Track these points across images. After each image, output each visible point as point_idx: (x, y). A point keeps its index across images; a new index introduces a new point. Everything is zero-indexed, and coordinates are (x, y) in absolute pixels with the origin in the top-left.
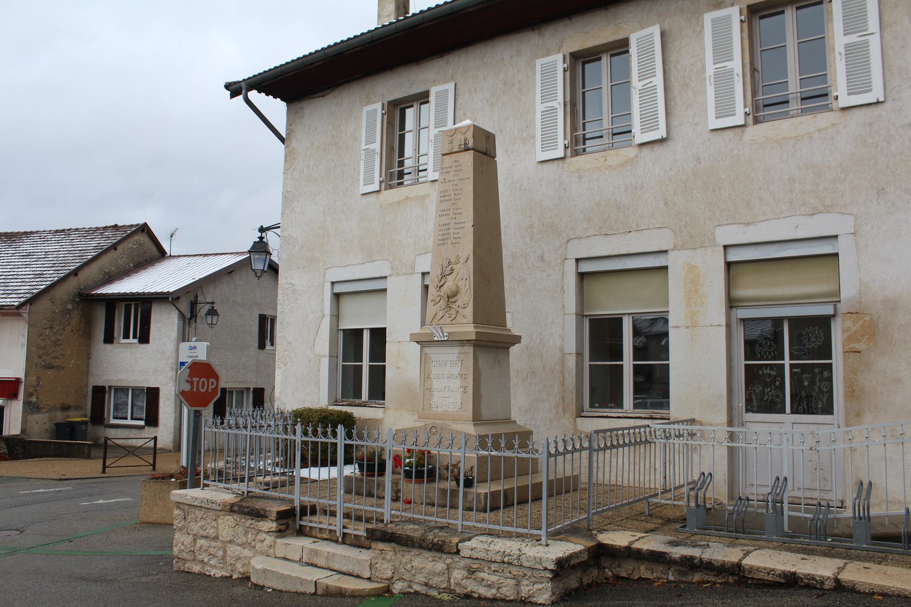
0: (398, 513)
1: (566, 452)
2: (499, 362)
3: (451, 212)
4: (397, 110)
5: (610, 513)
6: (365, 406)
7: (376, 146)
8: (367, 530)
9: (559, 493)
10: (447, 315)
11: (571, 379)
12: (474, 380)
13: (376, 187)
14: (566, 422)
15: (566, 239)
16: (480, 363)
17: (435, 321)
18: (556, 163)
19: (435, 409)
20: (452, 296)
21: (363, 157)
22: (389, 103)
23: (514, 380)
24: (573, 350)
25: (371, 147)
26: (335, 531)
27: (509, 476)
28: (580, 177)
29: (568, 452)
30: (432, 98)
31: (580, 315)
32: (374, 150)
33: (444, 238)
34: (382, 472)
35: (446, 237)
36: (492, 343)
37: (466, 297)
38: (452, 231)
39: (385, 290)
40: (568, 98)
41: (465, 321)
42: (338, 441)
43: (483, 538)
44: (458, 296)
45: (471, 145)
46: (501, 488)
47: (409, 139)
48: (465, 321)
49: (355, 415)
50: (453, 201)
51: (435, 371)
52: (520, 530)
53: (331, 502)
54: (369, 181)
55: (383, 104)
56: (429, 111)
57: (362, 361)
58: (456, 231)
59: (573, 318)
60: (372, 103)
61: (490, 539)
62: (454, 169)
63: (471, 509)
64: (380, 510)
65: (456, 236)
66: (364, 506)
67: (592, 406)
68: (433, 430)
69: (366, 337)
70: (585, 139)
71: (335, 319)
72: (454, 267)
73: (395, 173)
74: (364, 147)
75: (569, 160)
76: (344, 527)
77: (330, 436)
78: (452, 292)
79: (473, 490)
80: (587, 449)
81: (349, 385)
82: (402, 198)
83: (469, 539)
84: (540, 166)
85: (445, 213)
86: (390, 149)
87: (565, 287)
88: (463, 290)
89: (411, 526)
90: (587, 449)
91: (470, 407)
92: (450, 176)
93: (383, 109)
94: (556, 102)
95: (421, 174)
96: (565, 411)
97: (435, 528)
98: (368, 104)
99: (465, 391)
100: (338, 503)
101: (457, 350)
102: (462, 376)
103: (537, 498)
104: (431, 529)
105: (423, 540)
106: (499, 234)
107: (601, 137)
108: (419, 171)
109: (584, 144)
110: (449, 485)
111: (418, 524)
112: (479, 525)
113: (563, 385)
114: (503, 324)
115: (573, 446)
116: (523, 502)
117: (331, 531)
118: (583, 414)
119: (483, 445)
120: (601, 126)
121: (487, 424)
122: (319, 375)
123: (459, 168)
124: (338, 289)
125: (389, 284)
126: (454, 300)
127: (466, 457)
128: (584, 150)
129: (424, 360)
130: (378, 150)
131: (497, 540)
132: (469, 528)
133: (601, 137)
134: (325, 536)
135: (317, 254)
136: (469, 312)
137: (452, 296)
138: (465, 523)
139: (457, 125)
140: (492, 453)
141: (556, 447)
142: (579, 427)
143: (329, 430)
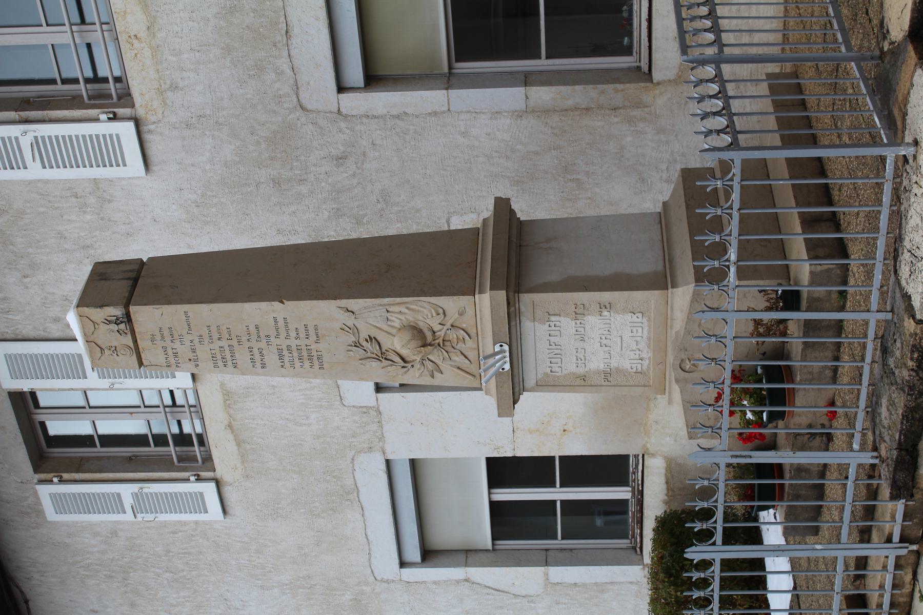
0: (858, 436)
1: (726, 111)
2: (548, 240)
3: (256, 346)
4: (53, 454)
5: (845, 11)
6: (641, 493)
7: (126, 491)
8: (894, 497)
9: (808, 122)
10: (461, 346)
11: (577, 95)
12: (586, 289)
13: (209, 489)
14: (660, 100)
15: (299, 112)
16: (554, 277)
17: (473, 369)
18: (147, 137)
19: (646, 363)
20: (422, 338)
21: (149, 517)
22: (37, 470)
23: (583, 208)
24: (520, 91)
25: (128, 501)
26: (898, 558)
27: (775, 223)
28: (174, 88)
29: (731, 124)
30: (25, 385)
31: (450, 80)
32: (135, 496)
33: (306, 357)
34: (776, 470)
35: (305, 353)
36: (512, 257)
37: (424, 310)
38: (293, 343)
39: (413, 462)
40: (12, 115)
41: (470, 312)
42: (718, 557)
43: (904, 270)
44: (422, 325)
45: (118, 312)
46: (801, 238)
47: (109, 427)
48: (470, 312)
49: (660, 512)
50: (234, 342)
51: (570, 366)
52: (886, 198)
53: (840, 567)
54: (198, 503)
55: (41, 482)
56: (51, 391)
57: (554, 502)
58: (293, 334)
59: (456, 94)
60: (38, 502)
61: (906, 256)
62: (168, 343)
63: (843, 294)
64: (852, 472)
65: (302, 335)
66: (843, 502)
67: (628, 51)
68: (688, 366)
69: (506, 495)
70: (96, 79)
71: (472, 558)
72: (364, 335)
73: (177, 451)
74: (129, 516)
75: (140, 112)
76: (889, 540)
77: (708, 573)
78: (413, 338)
79: (805, 291)
80: (718, 69)
81: (600, 527)
82: (230, 437)
83: (907, 298)
84: (154, 168)
85: (257, 357)
86: (133, 463)
87: (394, 112)
88: (410, 317)
89: (884, 411)
90: (718, 69)
91: (639, 296)
92: (183, 349)
93: (50, 481)
94: (21, 139)
95: (180, 400)
96: (639, 105)
97: (885, 364)
98: (40, 512)
99: (609, 307)
100: (840, 555)
101: (528, 325)
102: (578, 313)
103: (819, 167)
104: (888, 373)
105: (912, 388)
106: (297, 248)
107: (89, 46)
108: (174, 404)
109: (105, 80)
110: (795, 342)
111: (879, 397)
112: (878, 278)
113: (588, 109)
114: (473, 234)
115: (715, 96)
116: (826, 195)
117: (898, 566)
118: (645, 68)
119: (717, 277)
120: (65, 46)
121: (671, 261)
122: (584, 585)
123: (166, 333)
124: (413, 552)
125: (401, 454)
126: (429, 335)
127: (741, 305)
128: (118, 80)
129: (548, 384)
130: (135, 487)
131: (907, 243)
132: (883, 294)
133: (89, 46)
134: (908, 578)
135: (348, 597)
136: (451, 304)
137: (422, 338)
138: (874, 306)
139: (78, 334)
140: (733, 257)
141: (715, 114)
142: (671, 74)
143: (696, 575)
